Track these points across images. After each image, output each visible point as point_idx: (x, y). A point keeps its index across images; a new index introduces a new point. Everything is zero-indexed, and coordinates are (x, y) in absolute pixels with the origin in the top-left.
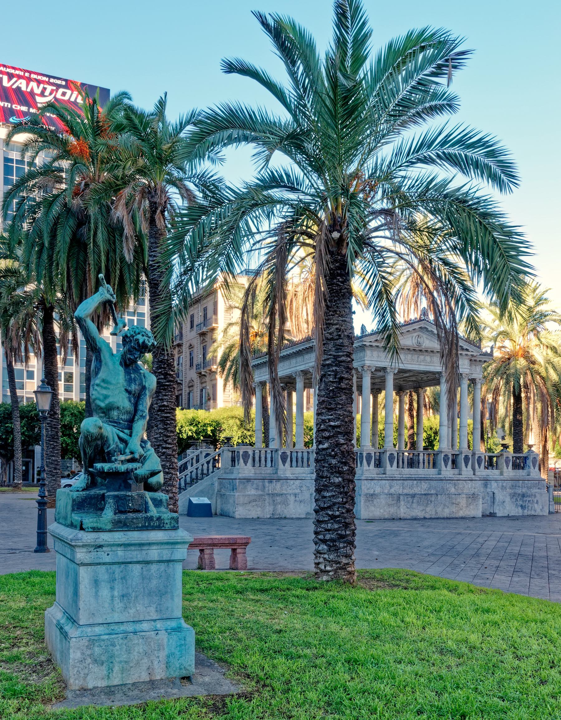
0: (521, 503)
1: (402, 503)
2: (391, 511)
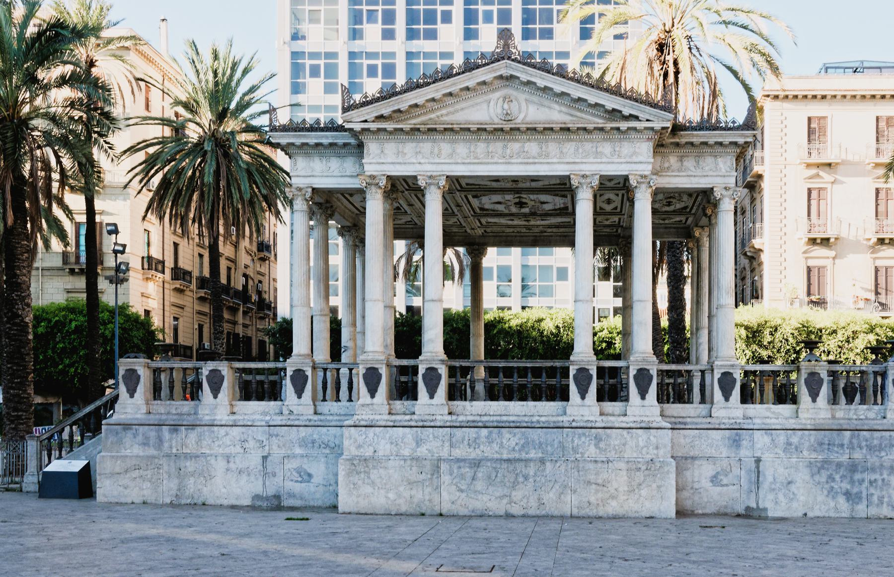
0: (846, 486)
1: (446, 478)
2: (421, 496)
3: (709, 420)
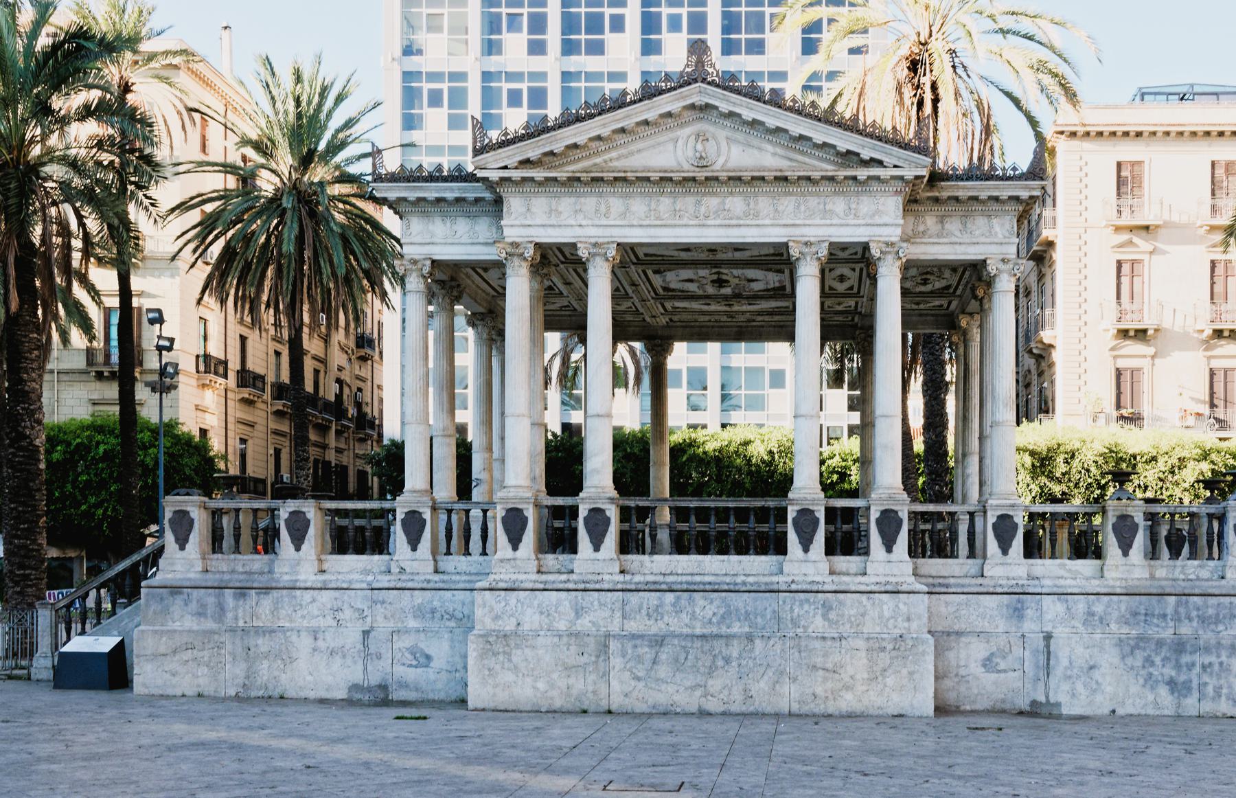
0: (1169, 672)
1: (616, 662)
2: (582, 687)
3: (980, 580)
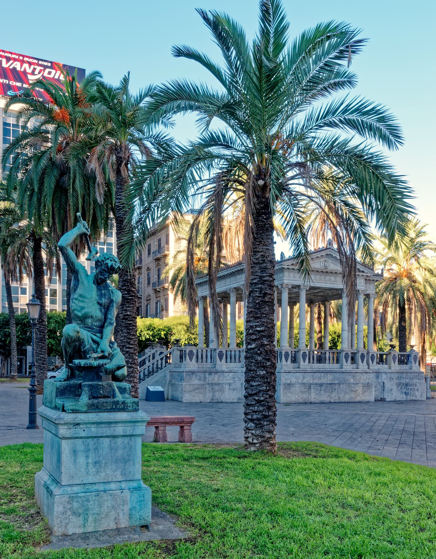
0: (405, 390)
1: (313, 390)
2: (304, 397)
